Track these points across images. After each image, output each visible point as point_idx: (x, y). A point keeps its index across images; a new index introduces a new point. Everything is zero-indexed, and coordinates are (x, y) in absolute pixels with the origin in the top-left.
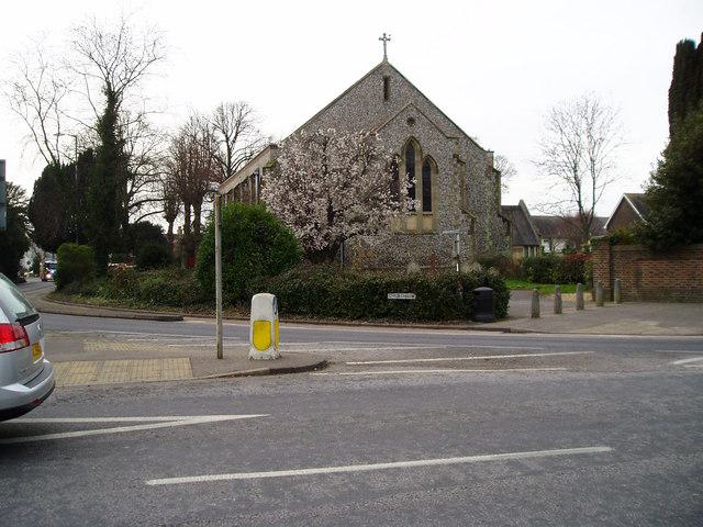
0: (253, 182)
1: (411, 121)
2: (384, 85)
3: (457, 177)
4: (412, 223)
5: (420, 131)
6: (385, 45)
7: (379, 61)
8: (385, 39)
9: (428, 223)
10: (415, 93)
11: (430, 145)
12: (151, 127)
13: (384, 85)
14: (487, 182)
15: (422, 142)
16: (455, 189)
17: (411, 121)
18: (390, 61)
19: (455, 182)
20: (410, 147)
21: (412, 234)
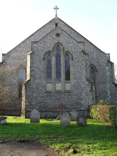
0: (58, 57)
1: (58, 35)
2: (56, 24)
3: (83, 62)
4: (59, 86)
5: (61, 39)
6: (56, 10)
7: (54, 17)
8: (56, 8)
9: (68, 87)
10: (69, 26)
11: (68, 45)
12: (50, 49)
13: (56, 24)
14: (107, 68)
15: (64, 44)
16: (83, 68)
17: (58, 35)
18: (59, 16)
19: (83, 65)
20: (58, 45)
21: (58, 92)
